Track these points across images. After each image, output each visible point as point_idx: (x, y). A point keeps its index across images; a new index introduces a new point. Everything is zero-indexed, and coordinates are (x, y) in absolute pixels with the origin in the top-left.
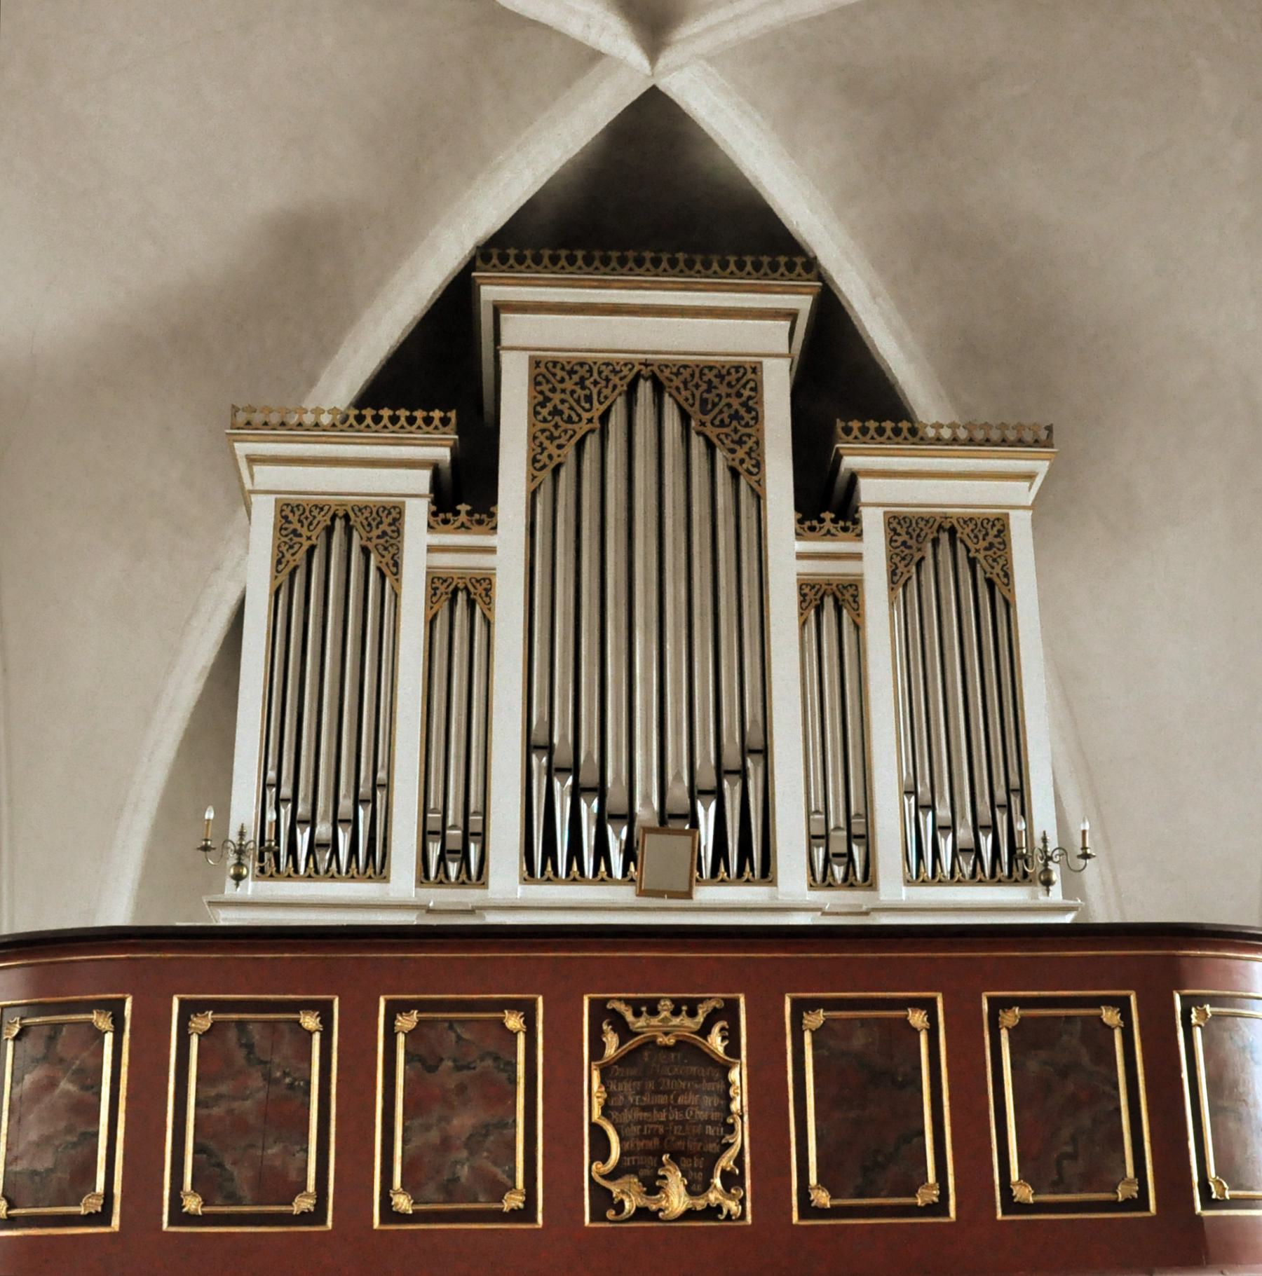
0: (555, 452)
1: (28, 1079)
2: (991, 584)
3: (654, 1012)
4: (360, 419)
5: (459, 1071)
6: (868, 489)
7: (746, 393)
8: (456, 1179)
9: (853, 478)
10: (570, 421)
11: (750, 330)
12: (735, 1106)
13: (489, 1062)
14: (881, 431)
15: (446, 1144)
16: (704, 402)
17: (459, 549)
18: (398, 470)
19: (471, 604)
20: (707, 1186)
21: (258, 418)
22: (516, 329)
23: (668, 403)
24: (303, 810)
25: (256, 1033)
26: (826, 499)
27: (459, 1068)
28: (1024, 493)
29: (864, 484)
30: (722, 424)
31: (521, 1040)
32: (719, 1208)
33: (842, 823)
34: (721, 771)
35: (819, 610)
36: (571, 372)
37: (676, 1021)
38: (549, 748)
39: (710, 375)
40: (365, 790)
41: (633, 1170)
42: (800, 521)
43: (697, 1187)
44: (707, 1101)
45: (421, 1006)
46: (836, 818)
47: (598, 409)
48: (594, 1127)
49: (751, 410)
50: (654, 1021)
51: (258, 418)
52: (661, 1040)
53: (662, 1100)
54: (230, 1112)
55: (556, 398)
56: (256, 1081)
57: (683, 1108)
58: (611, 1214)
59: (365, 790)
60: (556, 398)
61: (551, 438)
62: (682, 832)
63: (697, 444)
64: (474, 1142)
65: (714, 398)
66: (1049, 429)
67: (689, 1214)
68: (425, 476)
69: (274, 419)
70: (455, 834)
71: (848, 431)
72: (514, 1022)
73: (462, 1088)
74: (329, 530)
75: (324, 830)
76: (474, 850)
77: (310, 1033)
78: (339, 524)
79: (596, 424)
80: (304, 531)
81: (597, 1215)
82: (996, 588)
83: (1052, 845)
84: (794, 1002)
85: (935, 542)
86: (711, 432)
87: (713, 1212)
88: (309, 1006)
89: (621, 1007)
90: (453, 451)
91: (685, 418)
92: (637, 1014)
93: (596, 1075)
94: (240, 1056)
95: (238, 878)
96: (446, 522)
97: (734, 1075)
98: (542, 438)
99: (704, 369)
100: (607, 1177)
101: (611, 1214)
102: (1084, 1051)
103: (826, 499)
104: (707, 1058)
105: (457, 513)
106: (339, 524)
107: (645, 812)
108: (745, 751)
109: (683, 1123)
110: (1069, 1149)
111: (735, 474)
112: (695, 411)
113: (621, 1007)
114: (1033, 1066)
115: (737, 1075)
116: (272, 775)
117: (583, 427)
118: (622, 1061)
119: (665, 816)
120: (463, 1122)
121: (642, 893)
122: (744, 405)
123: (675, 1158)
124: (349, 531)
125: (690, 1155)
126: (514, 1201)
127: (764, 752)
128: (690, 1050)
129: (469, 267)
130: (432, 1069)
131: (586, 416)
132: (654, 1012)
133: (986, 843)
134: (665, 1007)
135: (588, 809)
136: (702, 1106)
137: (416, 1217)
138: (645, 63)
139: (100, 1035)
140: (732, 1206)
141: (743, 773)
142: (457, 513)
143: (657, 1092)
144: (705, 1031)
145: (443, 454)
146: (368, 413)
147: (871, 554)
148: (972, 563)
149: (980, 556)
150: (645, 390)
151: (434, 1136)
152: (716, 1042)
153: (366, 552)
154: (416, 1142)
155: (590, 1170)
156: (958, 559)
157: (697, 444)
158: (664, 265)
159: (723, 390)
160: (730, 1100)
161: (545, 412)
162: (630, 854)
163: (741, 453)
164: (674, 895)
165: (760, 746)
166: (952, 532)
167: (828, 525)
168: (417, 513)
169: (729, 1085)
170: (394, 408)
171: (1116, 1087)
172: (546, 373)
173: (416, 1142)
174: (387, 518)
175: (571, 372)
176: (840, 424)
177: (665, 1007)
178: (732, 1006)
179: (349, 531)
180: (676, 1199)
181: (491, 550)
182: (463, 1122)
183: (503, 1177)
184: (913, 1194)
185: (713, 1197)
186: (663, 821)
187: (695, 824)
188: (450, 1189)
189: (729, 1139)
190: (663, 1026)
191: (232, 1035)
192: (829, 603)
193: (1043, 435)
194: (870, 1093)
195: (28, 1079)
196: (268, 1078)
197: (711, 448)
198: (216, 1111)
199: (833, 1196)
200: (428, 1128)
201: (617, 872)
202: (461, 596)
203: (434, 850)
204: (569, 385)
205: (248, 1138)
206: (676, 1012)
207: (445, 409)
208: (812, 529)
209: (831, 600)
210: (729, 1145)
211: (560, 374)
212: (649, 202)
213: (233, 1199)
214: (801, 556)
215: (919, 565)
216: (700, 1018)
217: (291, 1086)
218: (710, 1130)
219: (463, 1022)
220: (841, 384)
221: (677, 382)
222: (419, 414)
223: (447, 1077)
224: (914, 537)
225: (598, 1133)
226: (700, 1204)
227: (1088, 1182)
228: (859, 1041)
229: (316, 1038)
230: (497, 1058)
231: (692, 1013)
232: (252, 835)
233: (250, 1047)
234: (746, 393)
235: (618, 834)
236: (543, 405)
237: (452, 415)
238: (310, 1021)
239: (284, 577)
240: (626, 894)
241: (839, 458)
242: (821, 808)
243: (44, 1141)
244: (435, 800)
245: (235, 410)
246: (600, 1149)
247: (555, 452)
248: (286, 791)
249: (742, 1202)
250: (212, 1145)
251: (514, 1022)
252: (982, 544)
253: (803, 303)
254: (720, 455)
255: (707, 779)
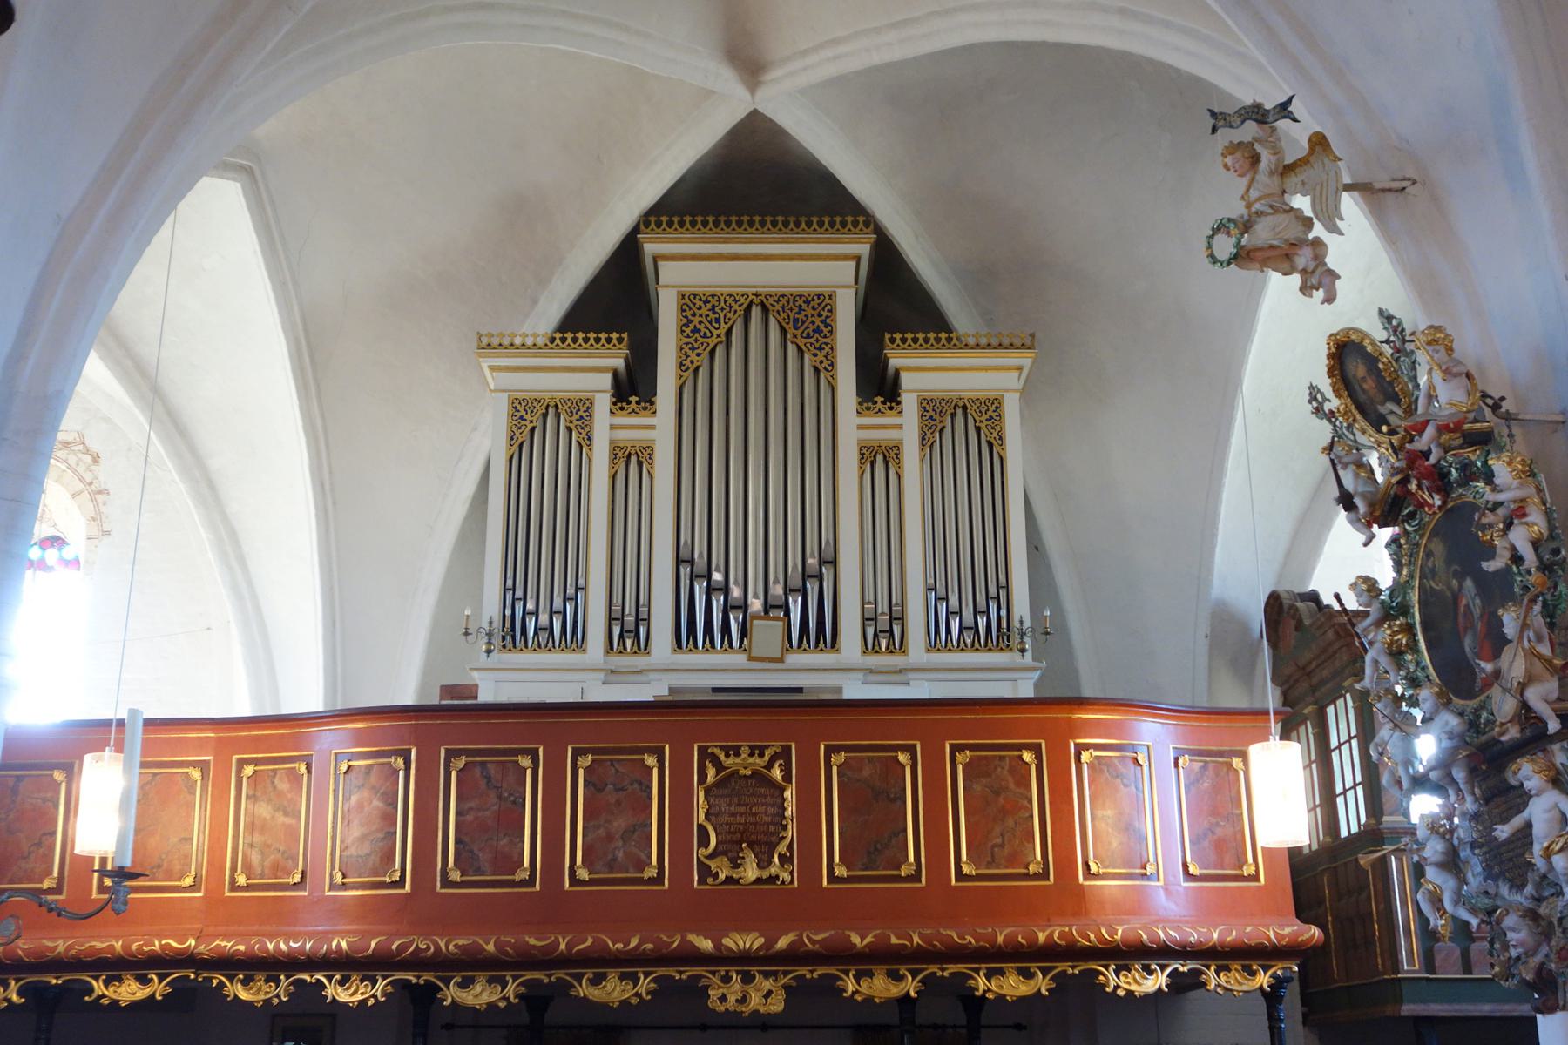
0: (695, 358)
1: (354, 799)
2: (990, 445)
3: (737, 754)
4: (563, 340)
5: (618, 795)
6: (907, 380)
7: (825, 313)
8: (614, 859)
9: (897, 373)
10: (705, 336)
11: (828, 269)
12: (788, 813)
13: (636, 786)
14: (915, 340)
15: (610, 838)
16: (796, 320)
17: (632, 427)
18: (590, 372)
19: (640, 464)
20: (770, 863)
21: (495, 341)
22: (671, 274)
23: (772, 321)
24: (530, 606)
25: (492, 769)
26: (879, 387)
27: (617, 790)
28: (1012, 381)
29: (904, 376)
30: (808, 336)
31: (655, 771)
32: (777, 877)
33: (886, 610)
34: (805, 576)
35: (873, 464)
36: (706, 302)
37: (751, 760)
38: (691, 562)
39: (800, 302)
40: (570, 591)
41: (725, 853)
42: (860, 404)
43: (763, 864)
44: (771, 810)
45: (594, 751)
46: (883, 606)
47: (724, 328)
48: (700, 826)
49: (826, 328)
50: (738, 760)
51: (495, 341)
52: (742, 772)
53: (743, 809)
54: (476, 818)
55: (696, 320)
56: (493, 798)
57: (755, 815)
58: (710, 880)
59: (570, 591)
60: (696, 320)
61: (693, 349)
62: (777, 619)
63: (791, 349)
64: (627, 834)
65: (803, 317)
66: (1032, 335)
67: (758, 881)
68: (608, 377)
69: (506, 342)
70: (629, 620)
71: (893, 340)
72: (651, 761)
73: (618, 803)
74: (545, 415)
75: (544, 619)
76: (642, 630)
77: (525, 770)
78: (551, 411)
79: (723, 338)
80: (527, 417)
81: (702, 881)
82: (993, 447)
83: (1027, 624)
84: (826, 747)
85: (953, 415)
86: (801, 342)
87: (773, 879)
88: (524, 752)
89: (717, 751)
90: (626, 360)
91: (783, 331)
92: (727, 756)
93: (702, 794)
94: (483, 783)
95: (489, 652)
96: (622, 409)
97: (787, 794)
98: (686, 349)
99: (795, 298)
100: (710, 857)
101: (710, 880)
102: (1010, 779)
103: (879, 387)
104: (772, 783)
105: (629, 403)
106: (551, 411)
107: (756, 605)
108: (822, 562)
109: (755, 824)
110: (999, 841)
111: (817, 370)
112: (790, 329)
113: (717, 751)
114: (977, 787)
115: (789, 794)
116: (510, 583)
117: (714, 340)
118: (717, 784)
119: (767, 607)
120: (620, 823)
121: (751, 659)
122: (823, 322)
123: (750, 845)
124: (558, 416)
125: (759, 843)
126: (651, 872)
127: (834, 563)
128: (761, 778)
129: (635, 230)
130: (601, 790)
131: (716, 332)
132: (737, 754)
133: (982, 622)
134: (745, 751)
135: (717, 602)
136: (765, 813)
137: (591, 882)
138: (748, 95)
139: (396, 772)
140: (786, 876)
141: (820, 577)
142: (629, 403)
143: (739, 805)
144: (769, 766)
145: (619, 363)
146: (569, 335)
147: (906, 426)
148: (978, 429)
149: (983, 426)
150: (756, 312)
151: (602, 832)
152: (777, 773)
153: (570, 430)
154: (590, 836)
155: (698, 853)
156: (968, 423)
157: (791, 349)
158: (769, 225)
159: (809, 311)
160: (784, 809)
161: (688, 331)
162: (744, 633)
163: (821, 357)
164: (772, 660)
165: (830, 558)
166: (965, 408)
167: (879, 405)
168: (603, 402)
169: (784, 800)
170: (586, 332)
171: (1031, 801)
172: (690, 303)
173: (590, 836)
174: (581, 409)
175: (706, 302)
176: (887, 336)
177: (745, 751)
178: (787, 749)
179: (558, 416)
180: (751, 872)
181: (652, 427)
182: (620, 823)
183: (644, 857)
184: (898, 868)
185: (773, 870)
186: (766, 611)
187: (787, 613)
188: (612, 865)
189: (783, 834)
190: (745, 763)
191: (478, 771)
192: (880, 458)
193: (1028, 343)
194: (873, 807)
195: (354, 799)
196: (500, 797)
197: (801, 352)
198: (470, 817)
199: (848, 869)
200: (598, 828)
201: (736, 643)
202: (632, 458)
203: (616, 631)
204: (704, 311)
205: (490, 829)
206: (751, 755)
207: (620, 332)
208: (868, 409)
209: (881, 457)
210: (783, 838)
211: (699, 303)
212: (755, 184)
213: (479, 871)
214: (860, 427)
215: (941, 431)
216: (767, 758)
217: (514, 802)
218: (772, 828)
219: (619, 761)
220: (897, 303)
221: (778, 307)
222: (603, 336)
223: (610, 795)
224: (936, 413)
225: (703, 830)
226: (765, 874)
227: (1013, 860)
228: (866, 772)
229: (529, 772)
230: (640, 784)
231: (762, 755)
232: (497, 623)
233: (489, 778)
234: (825, 313)
235: (736, 619)
236: (687, 325)
237: (625, 336)
238: (525, 762)
239: (515, 448)
240: (739, 659)
241: (887, 359)
242: (872, 599)
243: (363, 838)
244: (617, 598)
245: (480, 336)
246: (704, 842)
247: (695, 358)
248: (519, 594)
249: (792, 873)
250: (466, 839)
251: (651, 761)
252: (985, 417)
253: (864, 249)
254: (807, 357)
255: (796, 581)
